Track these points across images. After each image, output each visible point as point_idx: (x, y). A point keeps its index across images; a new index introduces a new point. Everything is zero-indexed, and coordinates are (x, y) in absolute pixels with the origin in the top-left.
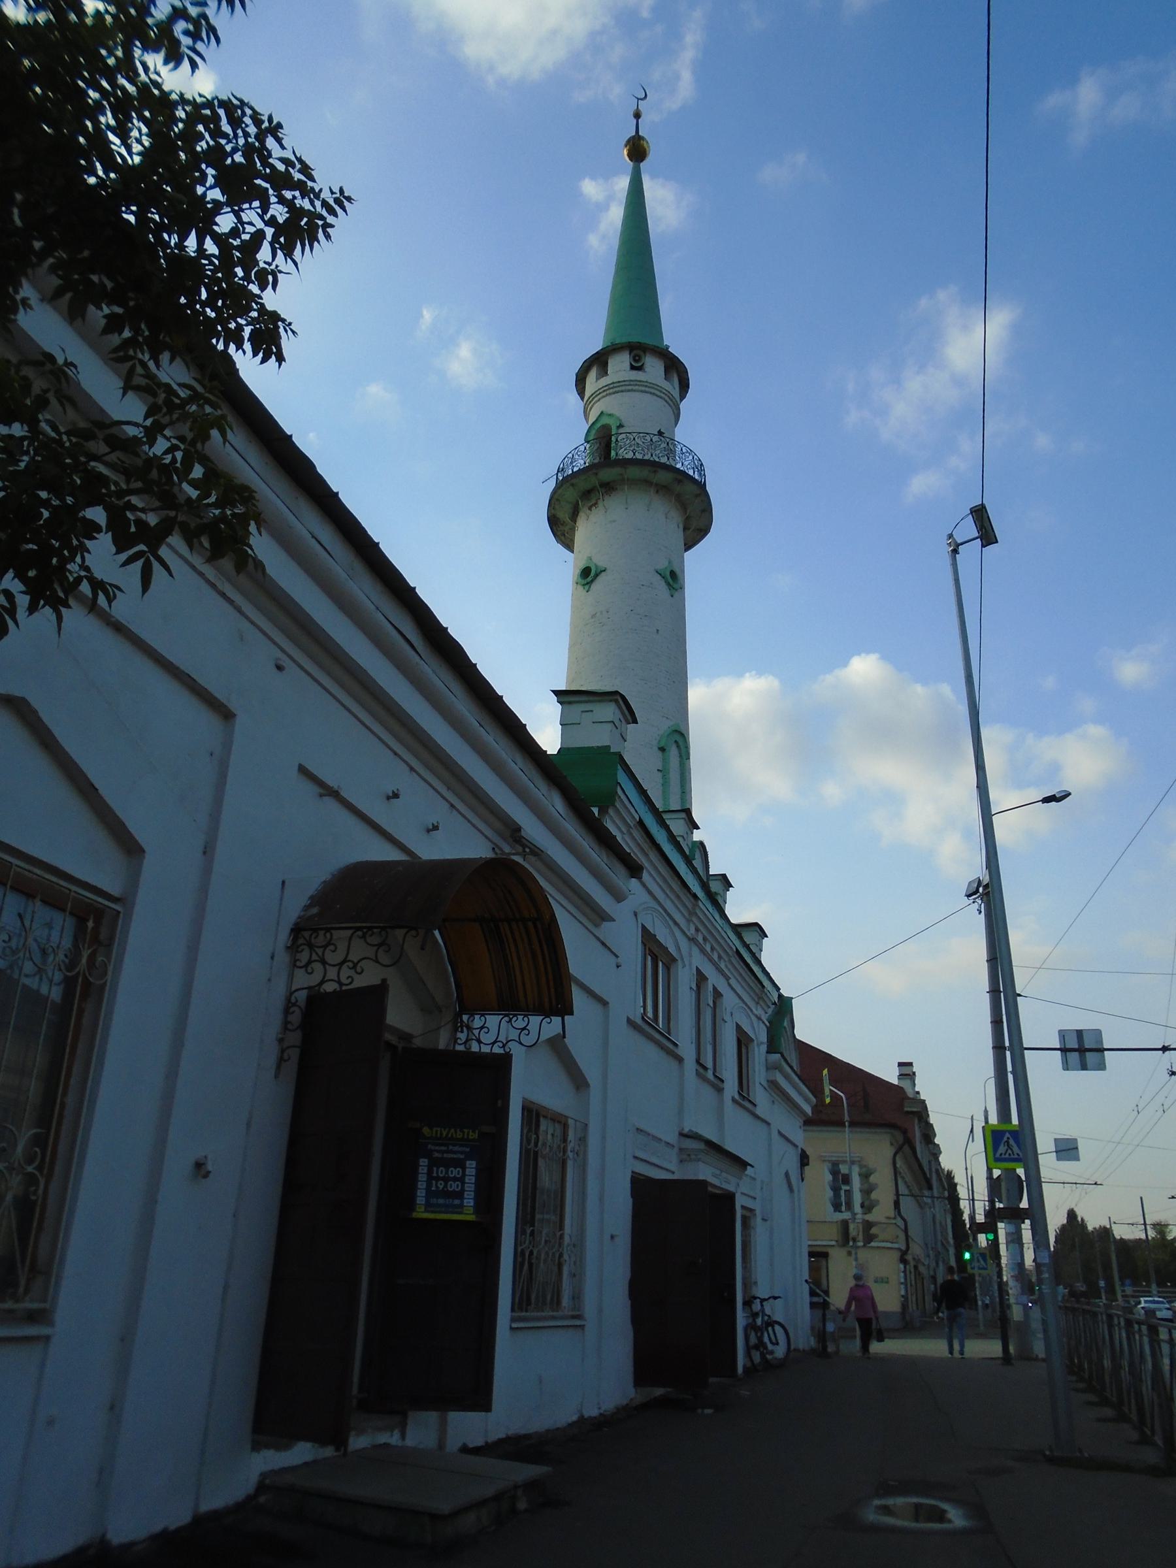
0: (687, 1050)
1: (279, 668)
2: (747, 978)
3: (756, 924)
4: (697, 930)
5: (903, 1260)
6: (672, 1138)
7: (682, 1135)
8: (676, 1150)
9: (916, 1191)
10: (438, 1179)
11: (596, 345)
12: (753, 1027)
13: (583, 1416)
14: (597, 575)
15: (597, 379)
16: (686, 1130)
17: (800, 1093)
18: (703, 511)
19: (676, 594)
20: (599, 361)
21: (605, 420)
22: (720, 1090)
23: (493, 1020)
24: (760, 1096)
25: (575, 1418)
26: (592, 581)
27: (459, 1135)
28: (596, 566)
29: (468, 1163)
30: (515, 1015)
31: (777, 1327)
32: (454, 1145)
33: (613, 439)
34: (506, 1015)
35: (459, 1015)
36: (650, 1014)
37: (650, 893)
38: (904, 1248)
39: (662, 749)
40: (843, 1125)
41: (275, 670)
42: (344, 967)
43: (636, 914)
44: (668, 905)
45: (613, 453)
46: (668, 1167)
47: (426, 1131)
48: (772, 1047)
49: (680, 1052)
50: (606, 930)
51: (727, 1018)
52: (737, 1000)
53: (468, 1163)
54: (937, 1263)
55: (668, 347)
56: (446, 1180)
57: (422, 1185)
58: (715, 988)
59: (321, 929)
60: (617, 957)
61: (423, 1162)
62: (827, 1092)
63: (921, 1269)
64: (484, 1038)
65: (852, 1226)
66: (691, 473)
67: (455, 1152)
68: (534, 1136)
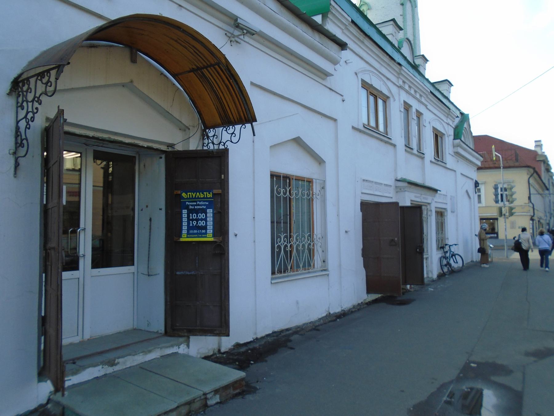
2: (439, 105)
3: (447, 80)
4: (404, 82)
5: (532, 219)
6: (391, 182)
7: (397, 180)
8: (393, 187)
9: (541, 191)
10: (193, 220)
12: (445, 129)
13: (330, 313)
16: (399, 178)
17: (473, 156)
22: (423, 158)
24: (450, 160)
25: (324, 315)
27: (202, 196)
29: (208, 210)
31: (457, 256)
32: (200, 201)
34: (224, 127)
35: (204, 130)
37: (367, 62)
38: (532, 214)
39: (402, 4)
40: (500, 168)
42: (35, 102)
43: (356, 74)
44: (377, 65)
46: (386, 195)
47: (184, 195)
48: (457, 136)
51: (427, 124)
52: (434, 116)
53: (208, 210)
54: (551, 218)
56: (197, 220)
57: (185, 224)
58: (417, 111)
60: (342, 96)
61: (185, 212)
62: (494, 155)
63: (541, 221)
64: (216, 141)
65: (503, 209)
67: (201, 205)
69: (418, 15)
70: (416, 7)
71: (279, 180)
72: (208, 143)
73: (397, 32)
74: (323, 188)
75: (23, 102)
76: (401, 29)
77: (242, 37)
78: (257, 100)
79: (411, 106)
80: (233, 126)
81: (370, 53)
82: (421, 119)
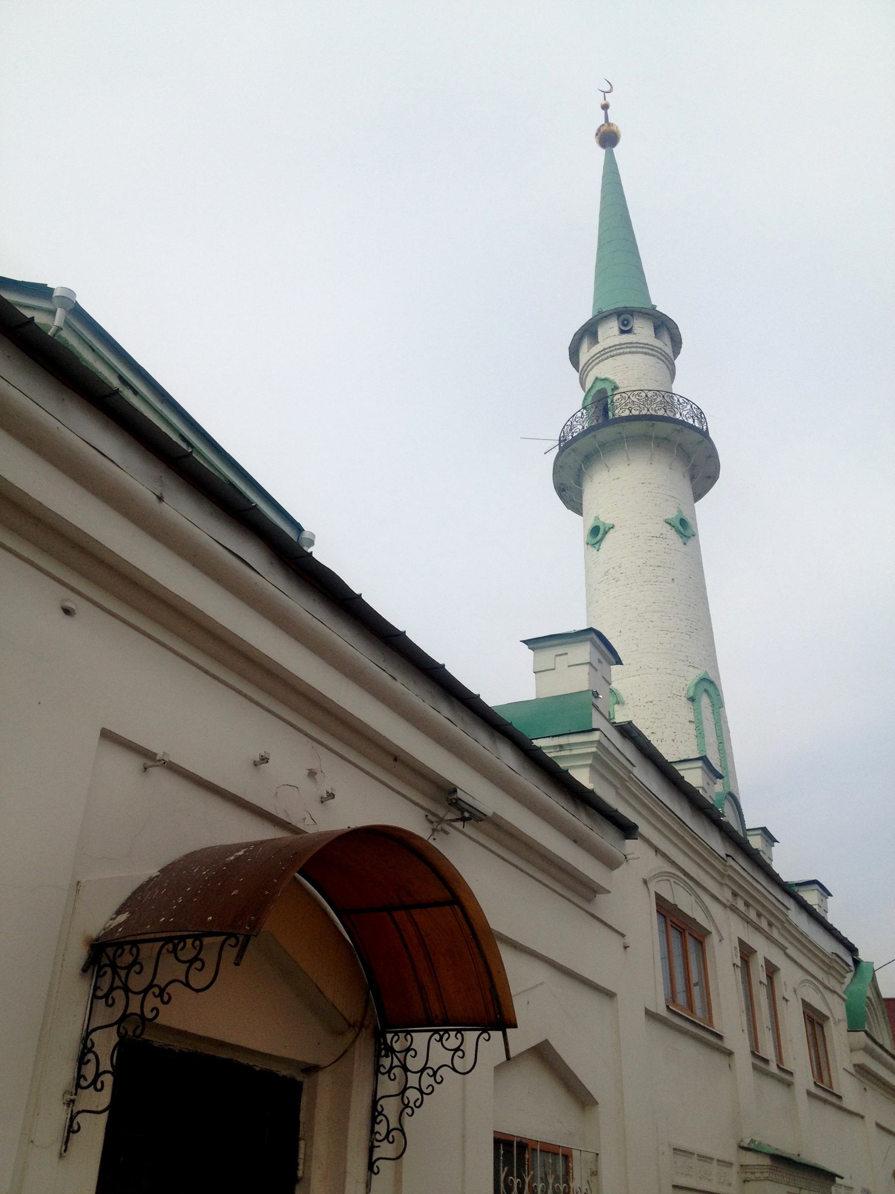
0: (736, 1038)
1: (67, 611)
3: (815, 882)
4: (735, 894)
6: (731, 1154)
11: (586, 314)
12: (827, 1005)
14: (606, 533)
15: (589, 349)
18: (709, 457)
19: (690, 543)
20: (589, 332)
21: (600, 385)
22: (789, 1085)
23: (420, 1039)
24: (847, 1086)
26: (601, 540)
28: (604, 524)
30: (446, 1031)
33: (609, 401)
34: (436, 1032)
36: (681, 998)
39: (692, 699)
41: (62, 613)
42: (150, 995)
43: (645, 882)
45: (610, 414)
49: (728, 1044)
50: (603, 905)
55: (654, 307)
58: (767, 962)
59: (189, 937)
60: (623, 935)
66: (690, 421)
68: (516, 1181)
69: (726, 722)
70: (722, 706)
71: (511, 1152)
72: (391, 1068)
73: (711, 783)
74: (594, 1173)
75: (112, 989)
76: (720, 777)
77: (459, 825)
78: (518, 973)
79: (752, 951)
80: (459, 1031)
81: (702, 864)
82: (751, 965)
